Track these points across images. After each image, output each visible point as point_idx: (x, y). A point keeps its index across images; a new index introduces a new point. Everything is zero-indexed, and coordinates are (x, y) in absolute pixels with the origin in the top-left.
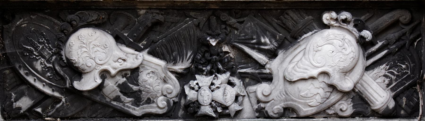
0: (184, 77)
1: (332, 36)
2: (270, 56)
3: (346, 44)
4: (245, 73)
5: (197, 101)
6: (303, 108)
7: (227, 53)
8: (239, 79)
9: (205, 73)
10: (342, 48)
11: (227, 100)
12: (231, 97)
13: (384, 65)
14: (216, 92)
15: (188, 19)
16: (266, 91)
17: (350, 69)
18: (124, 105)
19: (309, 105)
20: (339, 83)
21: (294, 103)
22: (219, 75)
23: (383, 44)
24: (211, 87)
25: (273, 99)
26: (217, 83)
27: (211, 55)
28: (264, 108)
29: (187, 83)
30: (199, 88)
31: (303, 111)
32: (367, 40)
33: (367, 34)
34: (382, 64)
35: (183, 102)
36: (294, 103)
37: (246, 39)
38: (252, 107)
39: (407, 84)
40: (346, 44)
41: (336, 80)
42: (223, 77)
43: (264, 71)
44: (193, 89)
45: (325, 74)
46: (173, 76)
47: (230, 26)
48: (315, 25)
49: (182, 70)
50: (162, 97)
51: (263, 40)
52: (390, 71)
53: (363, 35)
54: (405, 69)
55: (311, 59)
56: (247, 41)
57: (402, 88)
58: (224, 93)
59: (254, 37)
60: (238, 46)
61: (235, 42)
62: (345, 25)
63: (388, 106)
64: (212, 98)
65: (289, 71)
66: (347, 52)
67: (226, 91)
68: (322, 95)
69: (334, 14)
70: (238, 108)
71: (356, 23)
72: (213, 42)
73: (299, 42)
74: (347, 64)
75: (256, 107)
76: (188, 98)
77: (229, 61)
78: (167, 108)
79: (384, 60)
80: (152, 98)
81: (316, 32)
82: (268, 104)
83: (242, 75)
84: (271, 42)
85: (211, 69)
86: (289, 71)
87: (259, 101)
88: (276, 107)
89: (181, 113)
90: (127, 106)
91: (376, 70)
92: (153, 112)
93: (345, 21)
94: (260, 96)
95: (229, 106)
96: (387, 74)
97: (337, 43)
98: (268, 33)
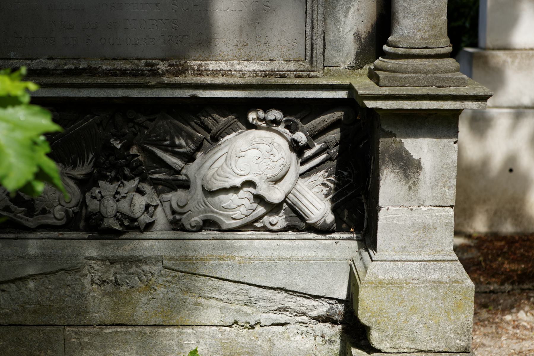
0: (86, 184)
1: (258, 140)
2: (187, 160)
3: (274, 149)
4: (157, 179)
5: (100, 212)
6: (224, 220)
7: (135, 155)
8: (151, 185)
9: (109, 180)
10: (270, 153)
11: (136, 211)
12: (140, 208)
13: (322, 172)
14: (122, 201)
15: (89, 116)
16: (181, 201)
17: (281, 177)
18: (15, 215)
19: (232, 218)
20: (267, 193)
21: (215, 215)
22: (125, 182)
23: (321, 147)
24: (116, 196)
25: (190, 210)
26: (123, 191)
27: (117, 159)
28: (180, 220)
29: (89, 189)
30: (102, 197)
31: (226, 224)
32: (300, 144)
33: (301, 137)
34: (320, 171)
35: (84, 211)
36: (215, 215)
37: (157, 141)
38: (167, 217)
39: (349, 194)
40: (274, 149)
41: (263, 189)
42: (132, 184)
43: (180, 177)
44: (95, 198)
45: (249, 183)
46: (71, 183)
47: (139, 125)
48: (240, 124)
49: (82, 176)
50: (59, 207)
51: (177, 142)
52: (329, 178)
53: (295, 138)
54: (347, 177)
55: (233, 166)
56: (159, 143)
57: (343, 198)
58: (131, 203)
59: (168, 138)
60: (148, 148)
61: (144, 143)
62: (274, 127)
63: (325, 221)
64: (117, 209)
65: (208, 179)
66: (276, 159)
67: (134, 200)
68: (247, 206)
69: (261, 114)
70: (149, 220)
71: (288, 124)
72: (118, 144)
73: (220, 145)
74: (276, 172)
75: (171, 217)
76: (89, 210)
77: (137, 166)
78: (65, 219)
79: (323, 165)
80: (48, 207)
81: (240, 133)
82: (185, 216)
83: (154, 181)
84: (186, 143)
85: (116, 175)
86: (208, 179)
87: (174, 212)
88: (193, 219)
89: (82, 224)
90: (19, 217)
91: (313, 178)
92: (49, 223)
93: (276, 122)
94: (175, 206)
95: (138, 218)
96: (325, 182)
97: (264, 147)
98: (183, 133)
